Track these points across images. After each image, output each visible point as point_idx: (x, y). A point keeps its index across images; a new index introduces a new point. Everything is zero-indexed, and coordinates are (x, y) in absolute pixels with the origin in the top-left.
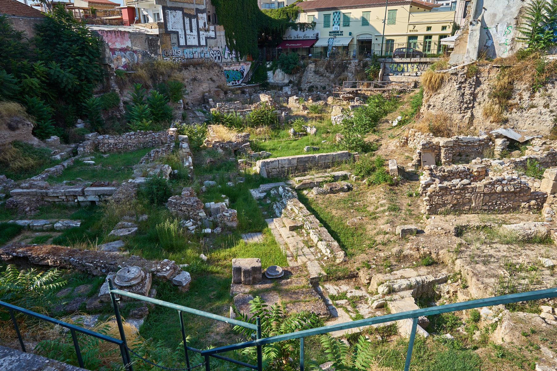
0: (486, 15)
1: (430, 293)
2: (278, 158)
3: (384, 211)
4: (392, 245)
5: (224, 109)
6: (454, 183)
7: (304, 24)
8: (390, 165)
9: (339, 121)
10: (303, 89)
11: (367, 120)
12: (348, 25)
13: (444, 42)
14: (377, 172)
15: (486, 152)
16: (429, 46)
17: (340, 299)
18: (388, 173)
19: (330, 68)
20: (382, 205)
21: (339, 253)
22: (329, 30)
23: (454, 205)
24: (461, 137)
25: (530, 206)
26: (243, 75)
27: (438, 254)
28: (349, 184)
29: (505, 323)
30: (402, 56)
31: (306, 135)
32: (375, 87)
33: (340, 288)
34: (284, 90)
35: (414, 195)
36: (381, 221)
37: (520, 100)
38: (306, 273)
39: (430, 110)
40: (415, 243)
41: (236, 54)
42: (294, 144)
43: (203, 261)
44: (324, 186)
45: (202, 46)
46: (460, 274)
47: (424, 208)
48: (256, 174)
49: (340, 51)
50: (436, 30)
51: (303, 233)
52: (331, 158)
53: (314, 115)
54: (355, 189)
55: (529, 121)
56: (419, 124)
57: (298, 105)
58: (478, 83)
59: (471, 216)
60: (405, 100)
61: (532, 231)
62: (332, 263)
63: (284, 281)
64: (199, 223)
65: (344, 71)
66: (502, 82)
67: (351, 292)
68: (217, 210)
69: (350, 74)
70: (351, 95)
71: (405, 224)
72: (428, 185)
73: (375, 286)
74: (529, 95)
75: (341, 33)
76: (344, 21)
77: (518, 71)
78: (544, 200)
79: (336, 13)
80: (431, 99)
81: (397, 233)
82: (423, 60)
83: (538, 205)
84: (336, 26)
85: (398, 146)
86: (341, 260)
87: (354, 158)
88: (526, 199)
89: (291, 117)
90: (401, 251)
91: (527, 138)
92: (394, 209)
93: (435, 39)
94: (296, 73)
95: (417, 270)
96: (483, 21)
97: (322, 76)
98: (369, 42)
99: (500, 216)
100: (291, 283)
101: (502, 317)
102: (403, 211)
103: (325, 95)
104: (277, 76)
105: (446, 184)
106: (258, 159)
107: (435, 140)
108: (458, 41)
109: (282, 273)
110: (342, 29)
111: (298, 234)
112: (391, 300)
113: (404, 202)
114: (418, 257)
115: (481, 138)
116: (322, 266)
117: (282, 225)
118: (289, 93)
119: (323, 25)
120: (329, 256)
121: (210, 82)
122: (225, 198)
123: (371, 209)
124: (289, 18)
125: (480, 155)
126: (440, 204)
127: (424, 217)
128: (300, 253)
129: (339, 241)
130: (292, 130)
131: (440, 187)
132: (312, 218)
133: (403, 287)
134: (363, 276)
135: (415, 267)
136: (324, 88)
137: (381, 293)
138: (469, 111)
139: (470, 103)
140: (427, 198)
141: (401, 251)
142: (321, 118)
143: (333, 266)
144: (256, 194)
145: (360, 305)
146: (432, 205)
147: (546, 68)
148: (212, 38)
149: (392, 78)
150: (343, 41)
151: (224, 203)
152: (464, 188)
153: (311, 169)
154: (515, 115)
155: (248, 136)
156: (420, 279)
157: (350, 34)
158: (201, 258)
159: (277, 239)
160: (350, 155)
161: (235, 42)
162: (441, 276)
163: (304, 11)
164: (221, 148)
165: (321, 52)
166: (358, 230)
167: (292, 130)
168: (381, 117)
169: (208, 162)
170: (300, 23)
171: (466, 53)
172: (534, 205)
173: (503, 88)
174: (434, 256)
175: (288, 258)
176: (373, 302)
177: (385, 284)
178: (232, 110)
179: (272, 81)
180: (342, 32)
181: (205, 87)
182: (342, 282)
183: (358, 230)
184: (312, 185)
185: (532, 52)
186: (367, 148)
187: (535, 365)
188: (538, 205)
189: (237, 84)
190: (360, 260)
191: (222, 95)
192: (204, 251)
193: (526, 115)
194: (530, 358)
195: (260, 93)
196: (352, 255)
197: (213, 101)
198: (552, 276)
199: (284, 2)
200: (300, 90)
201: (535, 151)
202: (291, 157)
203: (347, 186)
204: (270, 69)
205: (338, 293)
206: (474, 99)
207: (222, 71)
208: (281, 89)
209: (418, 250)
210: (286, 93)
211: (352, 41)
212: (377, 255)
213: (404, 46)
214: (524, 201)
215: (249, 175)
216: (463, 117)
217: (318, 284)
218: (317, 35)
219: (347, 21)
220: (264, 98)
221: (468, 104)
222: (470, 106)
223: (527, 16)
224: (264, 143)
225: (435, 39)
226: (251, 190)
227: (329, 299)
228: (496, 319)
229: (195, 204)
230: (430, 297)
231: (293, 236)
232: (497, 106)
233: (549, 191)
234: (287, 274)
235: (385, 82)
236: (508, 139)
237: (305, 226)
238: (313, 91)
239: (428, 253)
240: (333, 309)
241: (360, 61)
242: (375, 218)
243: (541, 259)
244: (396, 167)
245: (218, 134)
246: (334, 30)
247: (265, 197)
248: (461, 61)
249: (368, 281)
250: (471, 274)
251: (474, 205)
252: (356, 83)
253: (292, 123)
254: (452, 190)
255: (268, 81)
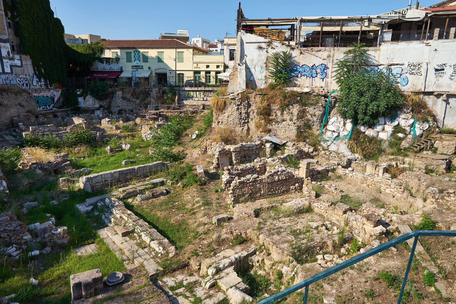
0: (248, 59)
1: (246, 265)
2: (101, 173)
3: (200, 207)
4: (211, 233)
5: (38, 132)
6: (248, 178)
7: (110, 58)
8: (198, 169)
9: (149, 137)
10: (113, 112)
11: (172, 135)
12: (147, 62)
13: (220, 76)
14: (188, 176)
15: (261, 153)
16: (210, 79)
17: (178, 289)
18: (197, 176)
19: (135, 94)
20: (197, 202)
21: (170, 248)
22: (130, 64)
23: (250, 194)
24: (244, 144)
25: (295, 188)
26: (54, 101)
27: (246, 234)
28: (167, 188)
29: (300, 275)
30: (191, 86)
31: (122, 150)
32: (174, 109)
33: (176, 278)
34: (95, 113)
35: (219, 190)
36: (199, 215)
37: (276, 116)
38: (145, 272)
39: (220, 126)
40: (229, 228)
41: (45, 82)
42: (112, 159)
43: (34, 286)
44: (147, 192)
45: (7, 73)
46: (264, 245)
47: (229, 200)
48: (80, 190)
49: (142, 81)
50: (213, 68)
51: (135, 236)
52: (148, 168)
53: (127, 134)
54: (172, 192)
55: (283, 130)
56: (214, 136)
57: (110, 126)
58: (249, 106)
59: (262, 201)
60: (198, 118)
61: (301, 205)
62: (166, 258)
63: (125, 285)
64: (24, 247)
65: (147, 97)
66: (264, 105)
67: (186, 280)
68: (45, 230)
69: (152, 100)
70: (155, 116)
71: (218, 214)
72: (229, 182)
73: (205, 270)
74: (280, 113)
75: (142, 68)
76: (143, 58)
77: (272, 97)
78: (303, 183)
79: (136, 51)
80: (219, 118)
81: (213, 223)
82: (207, 89)
83: (300, 186)
84: (137, 61)
85: (201, 154)
86: (174, 253)
87: (167, 166)
88: (293, 183)
89: (106, 136)
90: (219, 237)
91: (284, 142)
92: (207, 203)
93: (213, 74)
94: (106, 99)
95: (233, 249)
96: (246, 63)
97: (129, 101)
98: (165, 75)
99: (280, 198)
100: (132, 284)
101: (297, 271)
102: (214, 205)
103: (133, 117)
104: (88, 102)
105: (243, 179)
106: (80, 175)
107: (227, 147)
108: (232, 77)
109: (122, 277)
110: (143, 64)
111: (131, 238)
112: (220, 279)
113: (213, 197)
114: (232, 238)
115: (257, 143)
116: (158, 263)
117: (115, 233)
118: (101, 116)
119: (126, 60)
120: (163, 252)
121: (19, 107)
122: (51, 217)
123: (189, 206)
124: (95, 54)
125: (258, 155)
126: (241, 195)
127: (231, 206)
128: (136, 255)
129: (168, 238)
130: (109, 147)
131: (239, 182)
132: (141, 222)
133: (226, 265)
134: (194, 264)
135: (232, 247)
136: (132, 111)
137: (210, 275)
138: (246, 125)
139: (246, 119)
140: (231, 192)
141: (219, 237)
142: (133, 136)
143: (167, 260)
144: (82, 208)
145: (196, 289)
146: (235, 196)
147: (287, 95)
148: (18, 66)
149: (185, 102)
150: (145, 74)
151: (50, 222)
152: (255, 181)
153: (131, 179)
154: (273, 127)
155: (67, 155)
156: (238, 256)
157: (149, 68)
158: (32, 283)
159: (111, 247)
160: (163, 164)
161: (43, 71)
162: (251, 250)
163: (108, 49)
164: (40, 169)
165: (126, 82)
166: (182, 224)
167: (109, 147)
168: (182, 132)
169: (25, 183)
170: (104, 58)
171: (238, 85)
172: (298, 187)
173: (265, 108)
174: (243, 235)
175: (124, 262)
176: (206, 284)
177: (213, 266)
178: (48, 132)
179: (84, 106)
180: (142, 66)
181: (13, 112)
182: (177, 272)
183: (182, 224)
184: (135, 193)
185: (277, 85)
186: (176, 158)
187: (323, 299)
188: (300, 186)
189: (48, 108)
190: (189, 251)
191: (33, 119)
192: (34, 275)
193: (281, 126)
194: (319, 295)
195: (72, 116)
196: (182, 247)
197: (24, 125)
198: (318, 233)
199: (87, 40)
200: (111, 113)
201: (290, 150)
202: (113, 171)
203: (166, 190)
204: (80, 96)
205: (176, 283)
206: (248, 117)
207: (31, 97)
208: (93, 112)
209: (232, 233)
210: (98, 116)
211: (151, 73)
212: (202, 243)
213: (192, 79)
214: (292, 185)
215: (74, 191)
216: (243, 129)
217: (157, 280)
218: (122, 68)
219: (146, 59)
220: (77, 121)
221: (245, 120)
222: (246, 121)
223: (271, 62)
224: (82, 161)
225: (213, 74)
226: (78, 205)
227: (169, 291)
228: (293, 273)
229: (18, 228)
230: (246, 268)
231: (126, 241)
232: (263, 121)
233: (304, 176)
234: (127, 277)
235: (181, 105)
236: (273, 143)
237: (136, 230)
238: (122, 114)
239: (239, 234)
240: (175, 298)
241: (159, 89)
242: (194, 213)
243: (310, 223)
244: (202, 171)
245: (32, 156)
246: (135, 64)
247: (93, 210)
248: (236, 90)
249: (199, 267)
250: (271, 244)
251: (262, 192)
252: (158, 106)
253: (108, 141)
254: (247, 183)
255: (80, 106)
